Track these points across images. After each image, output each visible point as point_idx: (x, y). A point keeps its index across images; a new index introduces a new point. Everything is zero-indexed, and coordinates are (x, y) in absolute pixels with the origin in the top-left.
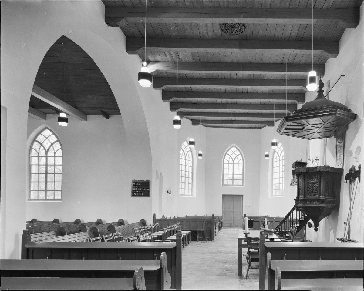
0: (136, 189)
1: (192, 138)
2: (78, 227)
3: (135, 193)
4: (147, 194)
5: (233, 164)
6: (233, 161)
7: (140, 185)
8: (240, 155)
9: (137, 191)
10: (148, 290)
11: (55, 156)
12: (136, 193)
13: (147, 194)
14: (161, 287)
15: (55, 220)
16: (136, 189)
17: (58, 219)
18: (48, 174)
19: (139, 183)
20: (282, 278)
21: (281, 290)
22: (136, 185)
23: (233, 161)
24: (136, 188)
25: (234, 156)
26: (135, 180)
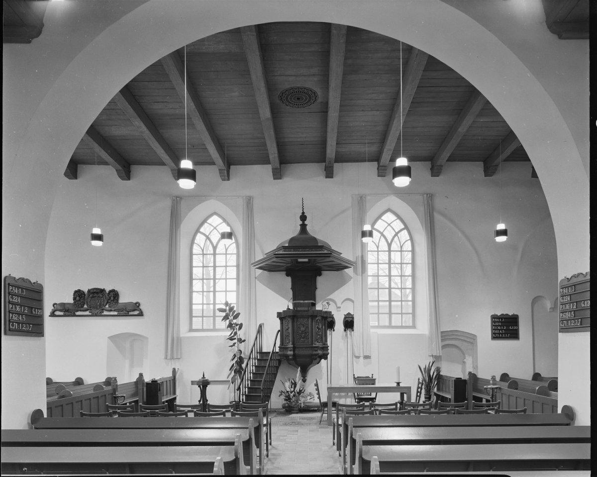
0: (499, 328)
1: (502, 223)
2: (54, 389)
3: (497, 333)
4: (513, 334)
5: (390, 251)
6: (389, 245)
7: (504, 322)
8: (405, 232)
9: (499, 330)
10: (228, 476)
11: (226, 254)
12: (499, 334)
13: (513, 334)
14: (236, 471)
15: (77, 379)
16: (499, 328)
17: (81, 377)
18: (217, 291)
19: (502, 319)
20: (363, 445)
21: (241, 474)
22: (497, 322)
23: (389, 245)
24: (499, 326)
25: (389, 235)
26: (495, 315)
